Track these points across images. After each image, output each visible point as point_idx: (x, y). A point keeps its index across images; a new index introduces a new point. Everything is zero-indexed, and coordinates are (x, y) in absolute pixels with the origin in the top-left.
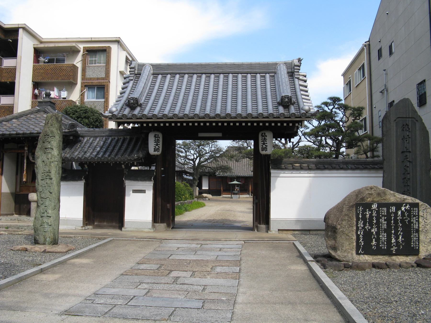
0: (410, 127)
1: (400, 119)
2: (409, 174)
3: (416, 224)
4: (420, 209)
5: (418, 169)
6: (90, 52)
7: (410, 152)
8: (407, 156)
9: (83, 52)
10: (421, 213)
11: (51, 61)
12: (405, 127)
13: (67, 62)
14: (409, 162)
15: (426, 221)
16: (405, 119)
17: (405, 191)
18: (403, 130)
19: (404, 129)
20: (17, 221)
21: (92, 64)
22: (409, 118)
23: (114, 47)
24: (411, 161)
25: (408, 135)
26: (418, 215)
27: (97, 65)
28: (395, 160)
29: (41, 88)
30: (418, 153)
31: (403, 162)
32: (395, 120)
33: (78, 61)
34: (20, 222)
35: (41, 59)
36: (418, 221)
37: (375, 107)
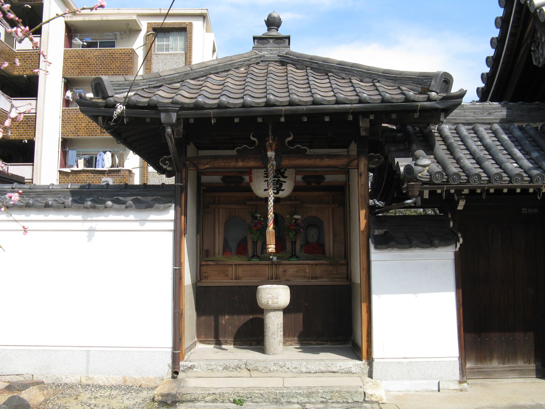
6: (160, 31)
9: (148, 32)
11: (91, 45)
13: (120, 47)
20: (245, 373)
21: (162, 50)
23: (197, 26)
27: (171, 52)
29: (77, 89)
33: (138, 45)
34: (254, 374)
35: (77, 41)
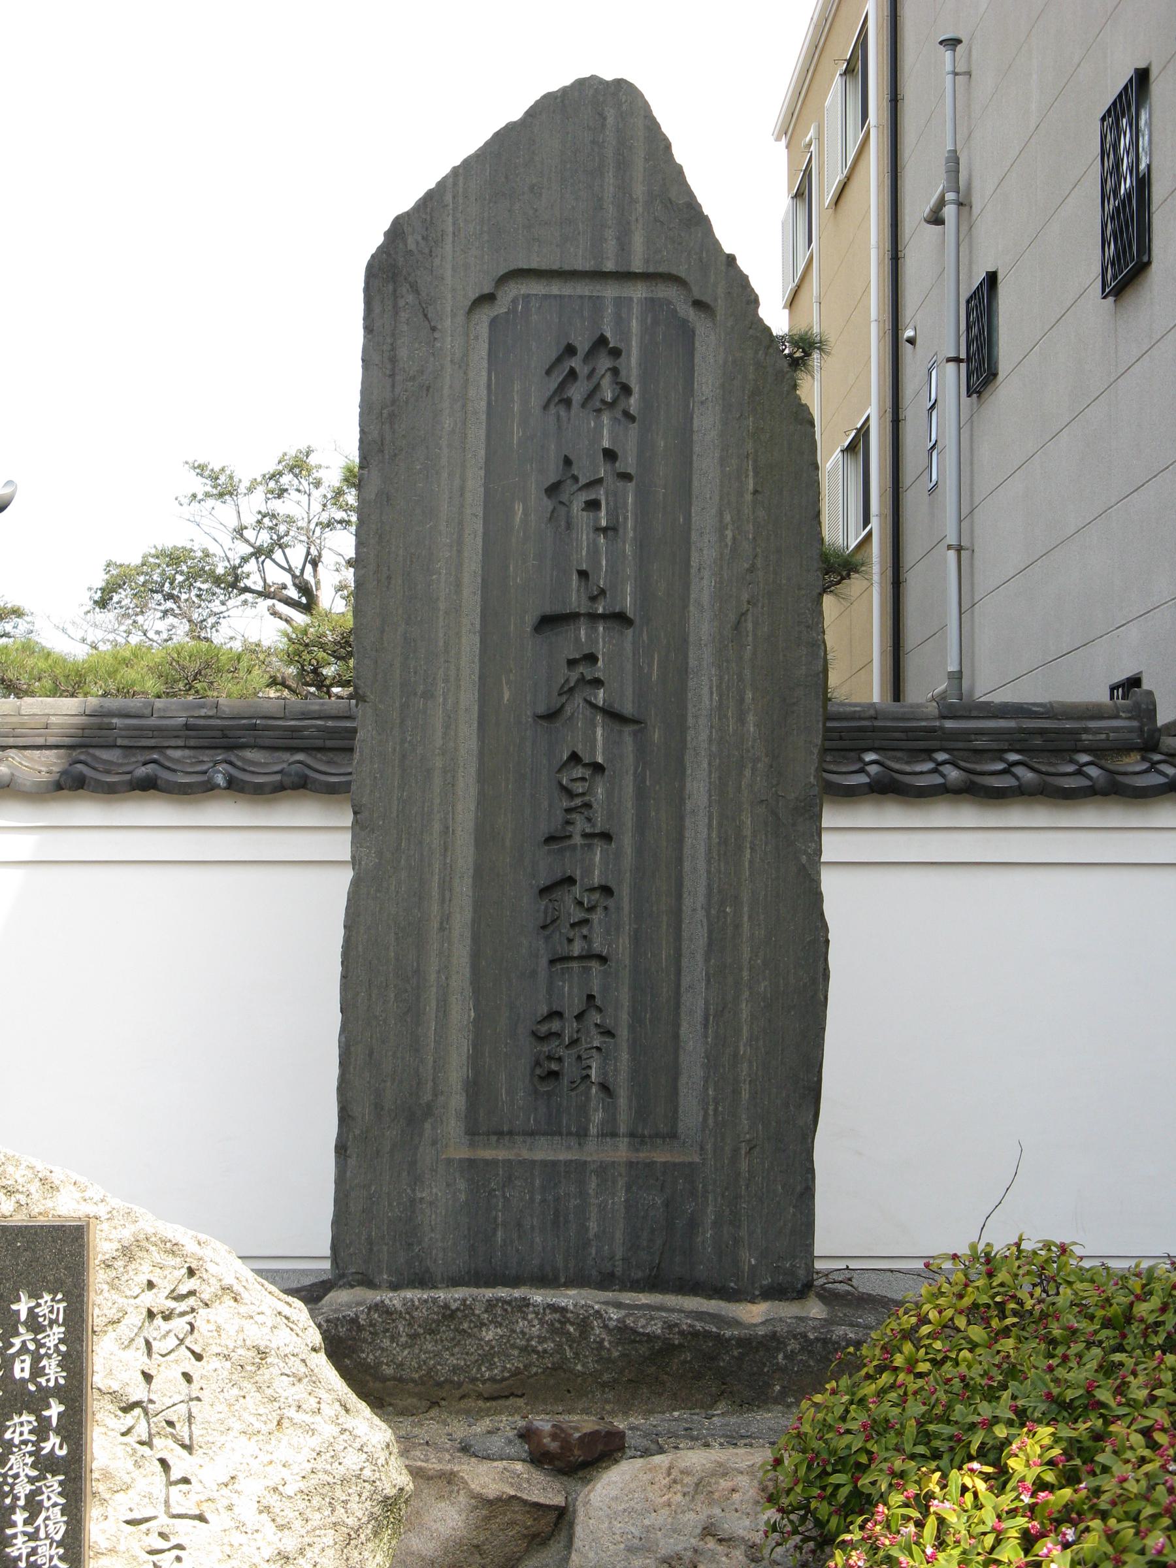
0: (632, 366)
1: (536, 288)
2: (606, 837)
3: (34, 1506)
4: (102, 1302)
5: (698, 788)
7: (621, 619)
8: (591, 658)
10: (112, 1363)
12: (582, 370)
14: (614, 716)
15: (181, 1464)
16: (583, 289)
17: (556, 1014)
18: (568, 402)
19: (577, 393)
22: (625, 276)
24: (628, 709)
25: (610, 455)
26: (74, 1392)
28: (468, 698)
30: (703, 627)
31: (552, 716)
32: (488, 298)
36: (72, 1470)
37: (911, 341)
